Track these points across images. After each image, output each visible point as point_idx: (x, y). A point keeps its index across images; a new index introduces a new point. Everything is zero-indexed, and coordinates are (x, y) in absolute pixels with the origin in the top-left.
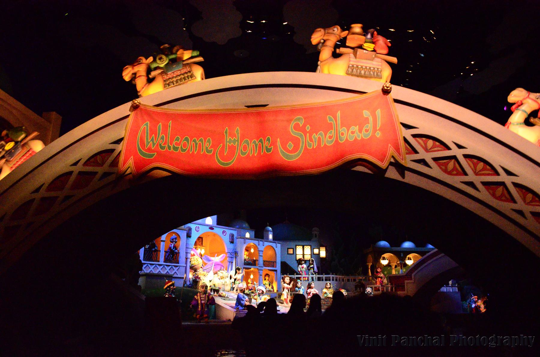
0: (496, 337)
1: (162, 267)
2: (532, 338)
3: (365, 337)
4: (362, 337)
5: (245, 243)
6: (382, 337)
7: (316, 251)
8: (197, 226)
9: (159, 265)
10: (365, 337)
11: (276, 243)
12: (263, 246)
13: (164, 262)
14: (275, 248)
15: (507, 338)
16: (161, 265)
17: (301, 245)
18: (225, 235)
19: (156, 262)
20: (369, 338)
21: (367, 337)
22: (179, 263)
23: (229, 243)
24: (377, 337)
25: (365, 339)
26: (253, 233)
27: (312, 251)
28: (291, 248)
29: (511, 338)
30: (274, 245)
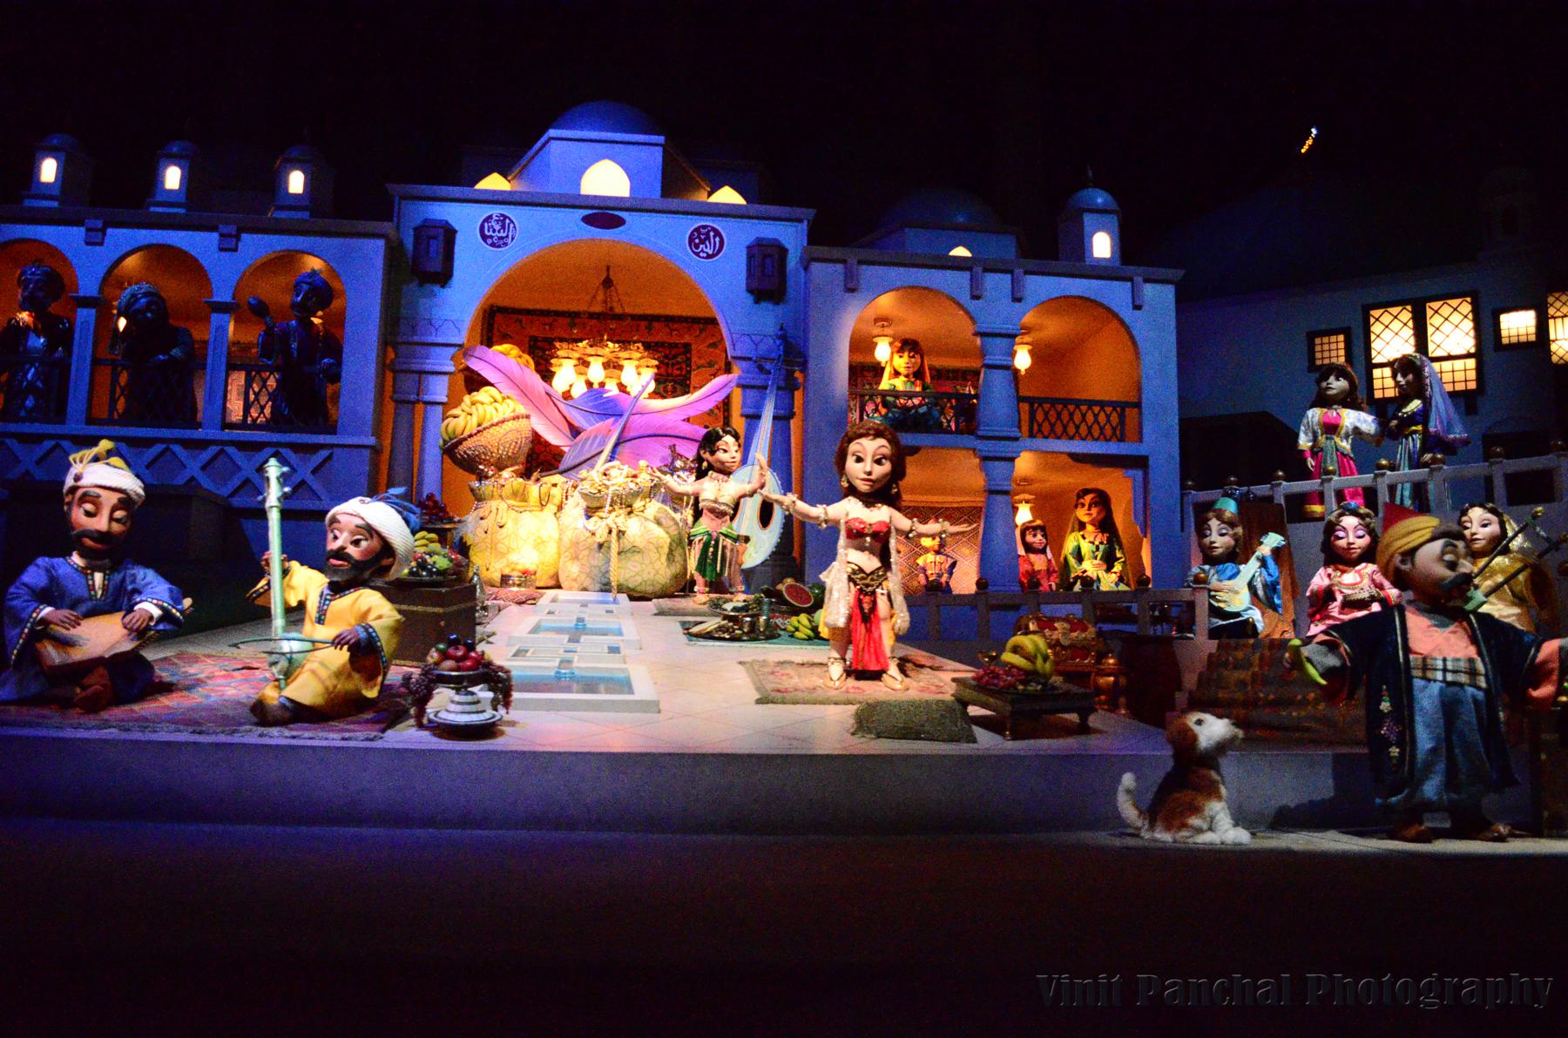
0: (1440, 979)
1: (206, 455)
2: (1546, 982)
3: (1060, 978)
4: (1050, 980)
5: (852, 290)
6: (1109, 981)
7: (1517, 324)
8: (496, 210)
9: (188, 444)
10: (1060, 978)
11: (1131, 280)
12: (1019, 300)
13: (1410, 468)
14: (1127, 314)
15: (1472, 983)
16: (203, 444)
17: (1400, 303)
18: (709, 257)
19: (138, 429)
20: (1072, 984)
21: (1064, 978)
22: (332, 430)
23: (749, 299)
24: (1096, 979)
25: (1059, 984)
26: (652, 157)
27: (1487, 321)
28: (1336, 332)
29: (1485, 984)
30: (1116, 294)
